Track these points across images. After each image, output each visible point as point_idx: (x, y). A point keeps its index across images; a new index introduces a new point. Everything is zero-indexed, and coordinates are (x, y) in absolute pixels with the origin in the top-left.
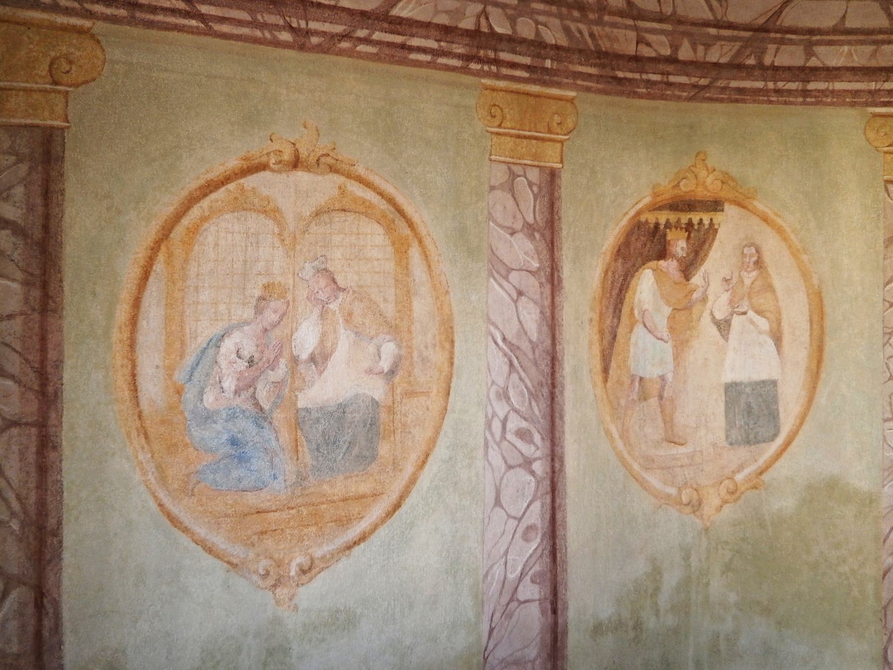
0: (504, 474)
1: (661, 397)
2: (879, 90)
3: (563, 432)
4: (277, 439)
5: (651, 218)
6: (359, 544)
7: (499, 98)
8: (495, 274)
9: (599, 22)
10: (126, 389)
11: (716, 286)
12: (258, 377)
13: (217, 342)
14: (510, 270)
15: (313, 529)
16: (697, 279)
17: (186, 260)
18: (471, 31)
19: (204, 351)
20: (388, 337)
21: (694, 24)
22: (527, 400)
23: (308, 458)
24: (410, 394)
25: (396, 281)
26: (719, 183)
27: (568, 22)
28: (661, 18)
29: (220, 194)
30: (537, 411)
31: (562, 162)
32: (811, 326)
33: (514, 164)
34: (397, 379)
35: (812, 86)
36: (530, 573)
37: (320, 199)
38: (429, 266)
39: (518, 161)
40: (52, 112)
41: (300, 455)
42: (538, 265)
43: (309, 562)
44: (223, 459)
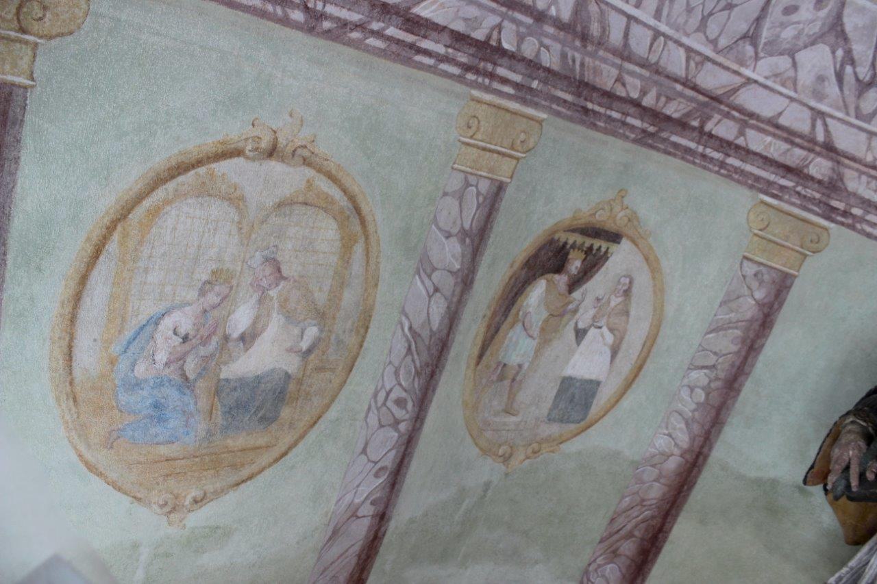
0: (376, 431)
1: (513, 380)
2: (775, 183)
3: (431, 401)
4: (196, 403)
5: (562, 237)
6: (246, 482)
7: (482, 111)
8: (421, 271)
9: (593, 55)
10: (61, 359)
11: (589, 301)
12: (188, 352)
13: (156, 321)
14: (434, 269)
15: (212, 472)
16: (577, 295)
17: (140, 243)
18: (481, 42)
19: (142, 328)
20: (314, 322)
21: (668, 77)
22: (412, 377)
23: (219, 418)
24: (320, 369)
25: (335, 273)
26: (626, 219)
27: (567, 49)
28: (644, 64)
29: (189, 178)
30: (416, 386)
31: (511, 177)
32: (643, 348)
33: (471, 174)
34: (312, 357)
35: (730, 161)
36: (371, 499)
37: (286, 191)
38: (368, 262)
39: (476, 172)
40: (14, 65)
41: (213, 417)
42: (459, 267)
43: (202, 495)
44: (144, 418)
